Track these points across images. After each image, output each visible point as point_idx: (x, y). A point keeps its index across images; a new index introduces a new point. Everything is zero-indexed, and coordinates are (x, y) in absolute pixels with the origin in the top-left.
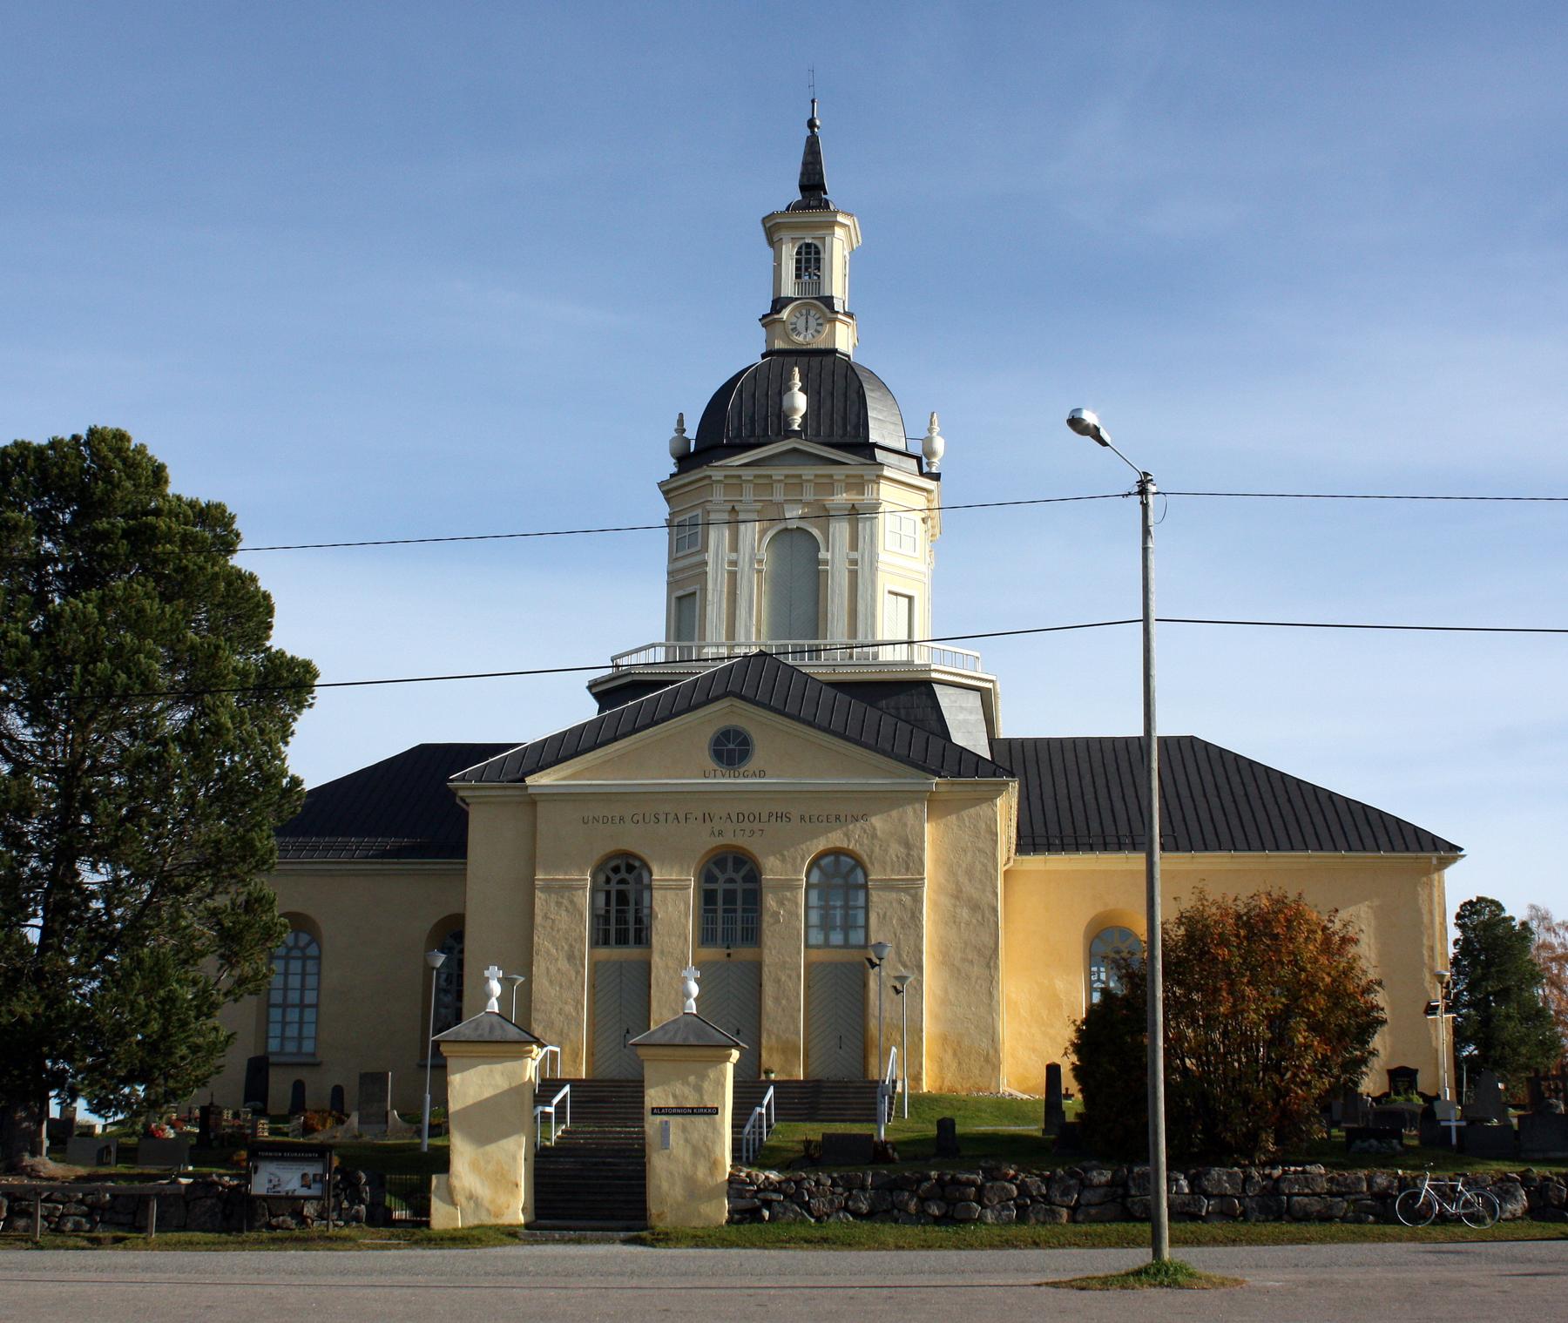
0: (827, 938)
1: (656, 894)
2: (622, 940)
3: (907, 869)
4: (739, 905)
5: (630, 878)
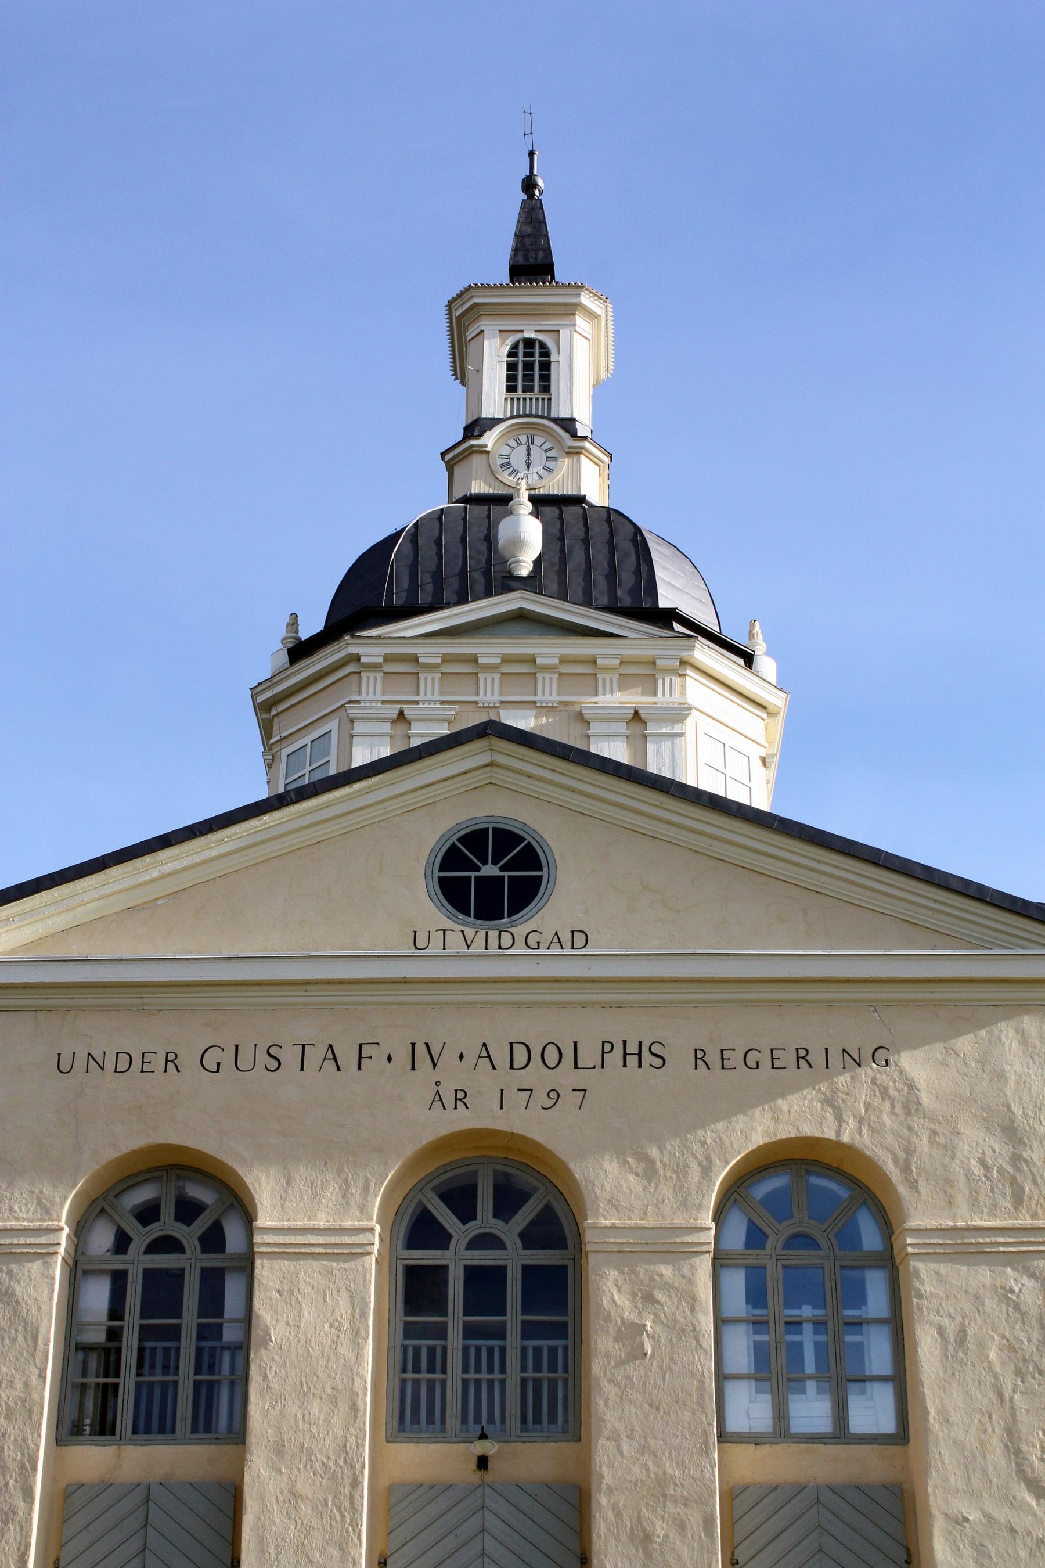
0: (781, 1415)
1: (265, 1271)
2: (154, 1423)
3: (1018, 1199)
4: (514, 1317)
5: (189, 1235)
